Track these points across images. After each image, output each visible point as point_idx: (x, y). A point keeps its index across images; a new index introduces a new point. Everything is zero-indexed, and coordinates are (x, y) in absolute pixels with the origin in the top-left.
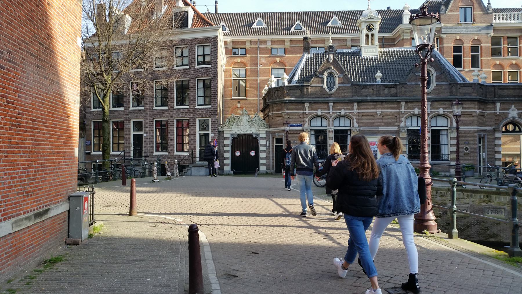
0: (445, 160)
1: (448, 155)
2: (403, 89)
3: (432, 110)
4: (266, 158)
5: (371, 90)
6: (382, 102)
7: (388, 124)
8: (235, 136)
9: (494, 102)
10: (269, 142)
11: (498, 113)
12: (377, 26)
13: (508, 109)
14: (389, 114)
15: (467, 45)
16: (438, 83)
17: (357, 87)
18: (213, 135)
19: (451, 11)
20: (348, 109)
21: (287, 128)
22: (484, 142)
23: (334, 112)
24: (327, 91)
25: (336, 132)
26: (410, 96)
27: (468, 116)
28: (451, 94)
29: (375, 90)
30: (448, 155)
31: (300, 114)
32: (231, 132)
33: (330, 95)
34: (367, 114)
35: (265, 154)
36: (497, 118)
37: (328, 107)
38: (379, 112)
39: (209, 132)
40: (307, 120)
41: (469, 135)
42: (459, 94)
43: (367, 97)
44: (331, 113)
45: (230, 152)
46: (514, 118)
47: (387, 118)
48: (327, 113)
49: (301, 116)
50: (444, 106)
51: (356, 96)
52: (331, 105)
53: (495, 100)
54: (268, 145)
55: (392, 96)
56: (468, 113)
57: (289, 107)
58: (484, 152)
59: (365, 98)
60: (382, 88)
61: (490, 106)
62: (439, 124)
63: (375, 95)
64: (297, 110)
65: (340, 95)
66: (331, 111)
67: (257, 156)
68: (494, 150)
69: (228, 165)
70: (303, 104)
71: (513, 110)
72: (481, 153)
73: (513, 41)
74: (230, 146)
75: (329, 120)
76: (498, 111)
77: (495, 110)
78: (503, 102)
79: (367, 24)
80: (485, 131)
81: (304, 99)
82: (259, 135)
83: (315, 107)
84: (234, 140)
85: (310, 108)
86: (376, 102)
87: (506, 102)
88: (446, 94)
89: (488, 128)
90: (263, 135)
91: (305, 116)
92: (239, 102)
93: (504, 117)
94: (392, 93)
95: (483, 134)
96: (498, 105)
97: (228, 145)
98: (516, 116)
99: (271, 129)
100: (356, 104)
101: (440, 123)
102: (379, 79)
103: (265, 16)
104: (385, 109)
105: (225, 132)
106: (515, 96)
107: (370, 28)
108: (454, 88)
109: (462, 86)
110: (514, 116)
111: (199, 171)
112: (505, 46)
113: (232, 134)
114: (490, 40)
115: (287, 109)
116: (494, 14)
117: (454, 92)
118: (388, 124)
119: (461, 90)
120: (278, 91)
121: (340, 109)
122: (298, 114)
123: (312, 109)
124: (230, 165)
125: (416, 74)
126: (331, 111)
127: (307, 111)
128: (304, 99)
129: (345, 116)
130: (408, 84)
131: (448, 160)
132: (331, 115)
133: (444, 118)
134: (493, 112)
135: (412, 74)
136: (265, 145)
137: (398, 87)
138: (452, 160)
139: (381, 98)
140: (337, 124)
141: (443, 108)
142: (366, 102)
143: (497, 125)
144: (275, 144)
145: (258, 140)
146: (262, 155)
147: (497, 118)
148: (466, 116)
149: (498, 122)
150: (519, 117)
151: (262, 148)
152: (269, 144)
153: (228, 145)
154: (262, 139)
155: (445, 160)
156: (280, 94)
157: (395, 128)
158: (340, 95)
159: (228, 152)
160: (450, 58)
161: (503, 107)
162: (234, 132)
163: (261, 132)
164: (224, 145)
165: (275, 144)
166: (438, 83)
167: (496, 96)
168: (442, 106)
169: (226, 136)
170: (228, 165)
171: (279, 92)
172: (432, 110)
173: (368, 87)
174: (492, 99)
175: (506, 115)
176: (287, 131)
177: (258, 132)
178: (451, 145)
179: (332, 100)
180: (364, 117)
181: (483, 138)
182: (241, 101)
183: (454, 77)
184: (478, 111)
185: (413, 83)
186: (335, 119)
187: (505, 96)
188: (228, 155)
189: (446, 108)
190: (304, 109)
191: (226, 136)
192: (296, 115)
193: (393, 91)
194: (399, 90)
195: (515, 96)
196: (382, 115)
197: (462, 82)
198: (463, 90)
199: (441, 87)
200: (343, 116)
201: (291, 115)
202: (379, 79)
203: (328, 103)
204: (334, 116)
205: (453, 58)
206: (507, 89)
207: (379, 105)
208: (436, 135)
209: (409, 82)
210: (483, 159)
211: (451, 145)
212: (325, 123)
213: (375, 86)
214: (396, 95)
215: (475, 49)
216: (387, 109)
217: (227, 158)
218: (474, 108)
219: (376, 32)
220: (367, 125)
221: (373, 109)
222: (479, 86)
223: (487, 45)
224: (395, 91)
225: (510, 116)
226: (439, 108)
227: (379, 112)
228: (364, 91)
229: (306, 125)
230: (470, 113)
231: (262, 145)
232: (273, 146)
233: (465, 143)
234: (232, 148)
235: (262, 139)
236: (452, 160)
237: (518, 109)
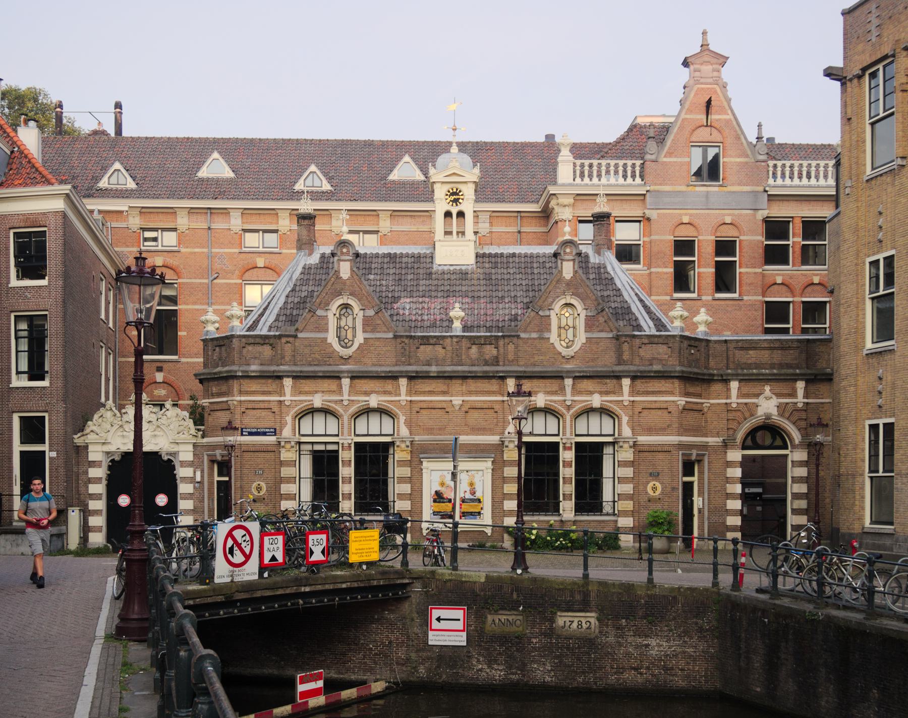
0: (608, 514)
1: (614, 502)
2: (511, 347)
3: (576, 398)
4: (194, 511)
5: (439, 348)
6: (464, 377)
7: (479, 429)
8: (117, 458)
9: (726, 381)
10: (202, 472)
11: (734, 405)
12: (468, 192)
13: (757, 396)
14: (479, 405)
15: (705, 242)
16: (590, 335)
17: (406, 341)
18: (54, 454)
19: (670, 154)
20: (385, 393)
21: (231, 439)
22: (701, 473)
23: (353, 401)
24: (336, 346)
25: (359, 447)
26: (526, 365)
27: (659, 412)
28: (620, 362)
29: (449, 348)
30: (614, 502)
31: (271, 405)
32: (107, 448)
33: (346, 360)
34: (431, 405)
35: (728, 523)
36: (731, 416)
37: (340, 387)
38: (457, 401)
39: (45, 447)
40: (289, 419)
41: (660, 456)
42: (637, 361)
43: (429, 365)
44: (345, 403)
45: (104, 497)
46: (768, 417)
47: (475, 415)
48: (336, 402)
49: (276, 409)
50: (604, 389)
51: (404, 364)
52: (346, 382)
53: (728, 375)
54: (198, 479)
55: (486, 363)
56: (658, 405)
57: (244, 388)
58: (701, 493)
59: (426, 368)
60: (464, 342)
61: (717, 387)
62: (594, 430)
63: (449, 361)
64: (264, 393)
65: (366, 360)
66: (346, 397)
67: (172, 506)
68: (725, 489)
69: (98, 529)
70: (277, 381)
71: (768, 398)
72: (695, 498)
73: (813, 228)
74: (104, 482)
75: (564, 422)
76: (734, 399)
77: (728, 397)
78: (744, 380)
79: (447, 187)
80: (705, 447)
81: (282, 368)
82: (175, 454)
83: (307, 389)
84: (114, 466)
85: (296, 391)
86: (451, 378)
87: (752, 379)
88: (607, 362)
89: (712, 440)
90: (186, 454)
91: (284, 409)
92: (160, 369)
93: (747, 414)
94: (487, 357)
95: (694, 452)
96: (734, 385)
97: (98, 480)
98: (774, 411)
99: (205, 440)
100: (403, 382)
101: (596, 429)
102: (457, 325)
103: (231, 148)
104: (470, 393)
105: (91, 448)
106: (772, 366)
107: (455, 196)
108: (626, 347)
109: (646, 341)
110: (769, 411)
111: (18, 545)
112: (795, 240)
113: (108, 453)
114: (761, 228)
115: (241, 393)
116: (771, 163)
117: (626, 356)
118: (479, 429)
119: (642, 352)
120: (220, 346)
121: (367, 393)
122: (266, 405)
123: (300, 393)
124: (104, 529)
125: (541, 313)
126: (346, 397)
127: (288, 397)
128: (282, 368)
129: (604, 411)
130: (523, 335)
131: (614, 514)
132: (569, 408)
133: (384, 416)
134: (724, 401)
135: (533, 314)
136: (192, 480)
137: (501, 343)
138: (624, 513)
139: (460, 368)
140: (582, 429)
141: (601, 393)
142: (426, 376)
143: (731, 432)
144: (217, 478)
145: (173, 468)
146: (184, 505)
147: (731, 416)
148: (653, 411)
149: (733, 425)
150: (781, 415)
151: (184, 488)
152: (202, 476)
153: (98, 480)
154: (184, 464)
155: (608, 514)
156: (224, 354)
157: (494, 439)
158: (366, 360)
159: (97, 497)
160: (665, 270)
161: (745, 390)
162: (112, 448)
163: (181, 448)
164: (90, 481)
165: (217, 478)
166: (590, 335)
167: (731, 366)
168: (598, 389)
169: (92, 457)
170: (98, 529)
171: (223, 349)
172: (576, 398)
173: (432, 341)
174: (721, 372)
175: (751, 410)
176: (232, 446)
177: (175, 448)
178: (622, 480)
179: (348, 372)
180: (424, 412)
181: (699, 461)
182: (165, 366)
183: (637, 319)
184: (682, 401)
185: (534, 335)
186: (577, 416)
187: (749, 366)
188: (99, 505)
189: (607, 393)
190: (281, 393)
191: (92, 457)
192: (262, 405)
193: (490, 351)
194: (501, 350)
195: (772, 366)
196: (464, 409)
197: (654, 332)
198: (647, 352)
199: (598, 343)
200: (540, 410)
201: (250, 406)
202: (457, 325)
203: (339, 378)
204: (353, 409)
205: (672, 270)
206: (755, 348)
207: (456, 385)
208: (590, 456)
209: (525, 331)
210: (700, 511)
211: (622, 480)
212: (552, 425)
213: (449, 340)
214: (496, 361)
215: (725, 247)
216: (477, 393)
217: (97, 512)
218: (671, 393)
219: (468, 206)
220: (430, 431)
221: (444, 393)
222: (686, 343)
223: (752, 239)
224: (495, 352)
225: (760, 412)
226: (591, 393)
227: (457, 401)
228: (425, 351)
229: (287, 432)
230: (664, 406)
231: (185, 479)
232: (211, 483)
233: (651, 474)
234: (108, 486)
235: (184, 464)
236: (624, 513)
237: (779, 395)
